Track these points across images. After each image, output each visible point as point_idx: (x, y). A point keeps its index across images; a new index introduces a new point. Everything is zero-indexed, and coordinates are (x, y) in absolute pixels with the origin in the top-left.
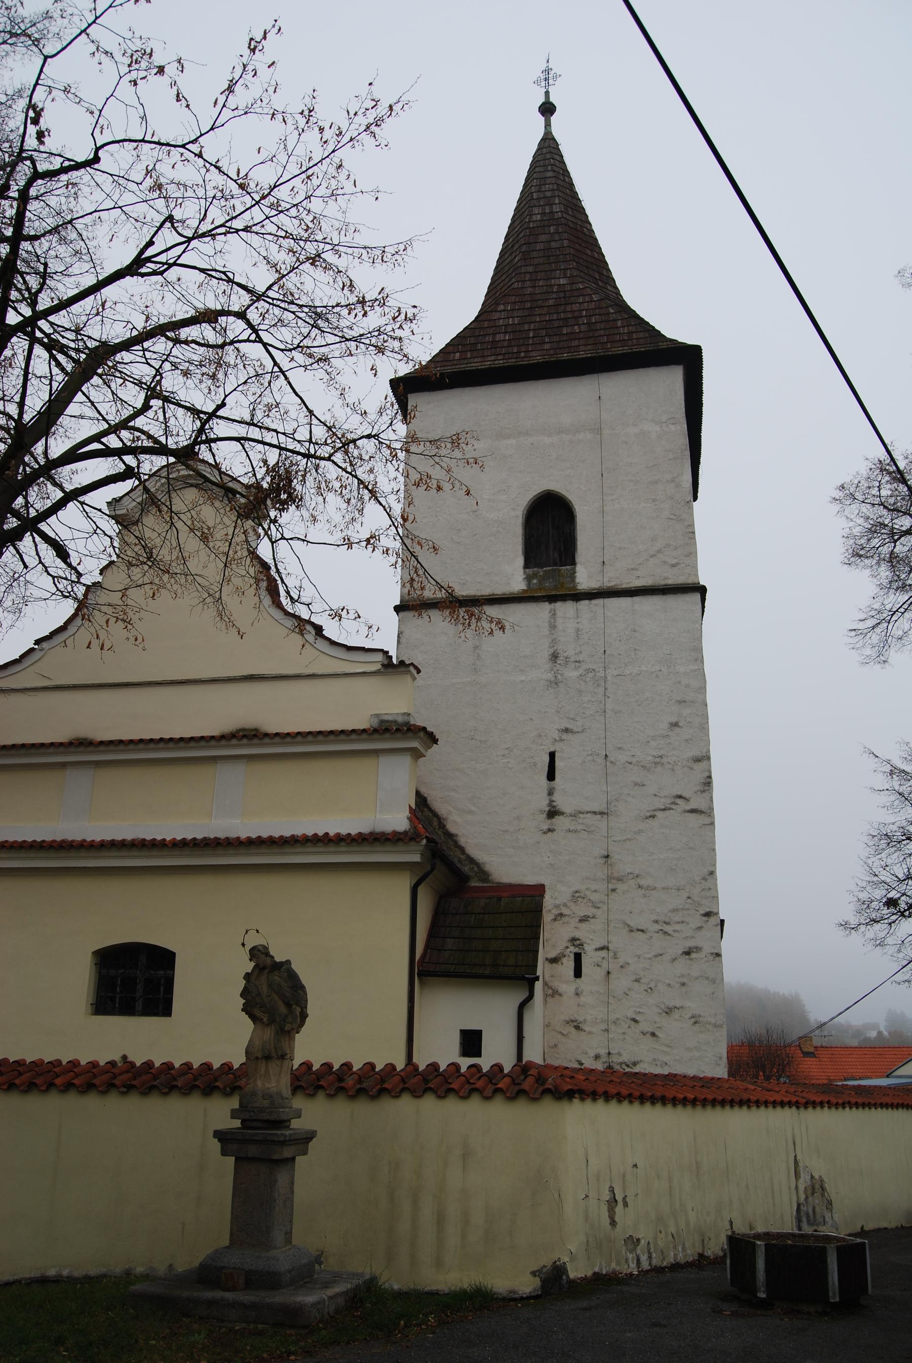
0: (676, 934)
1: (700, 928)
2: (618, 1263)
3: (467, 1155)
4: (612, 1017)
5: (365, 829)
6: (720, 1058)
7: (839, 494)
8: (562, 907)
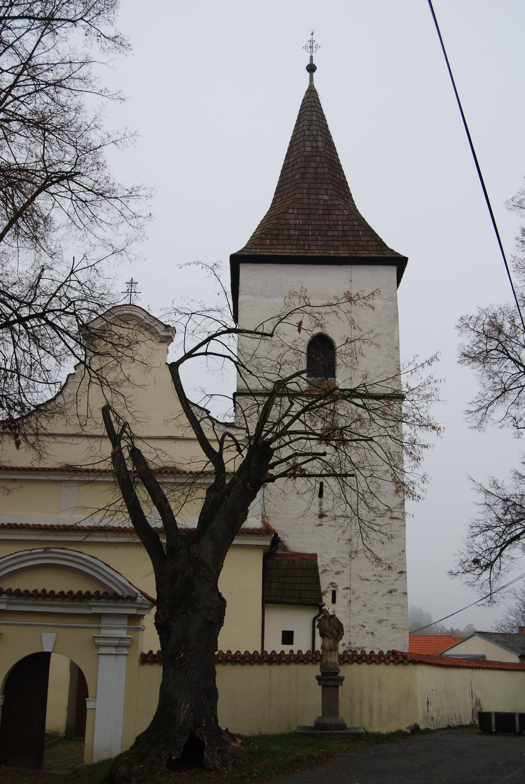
0: (384, 582)
1: (397, 579)
2: (430, 726)
3: (380, 686)
4: (352, 624)
6: (406, 646)
7: (458, 323)
8: (326, 566)
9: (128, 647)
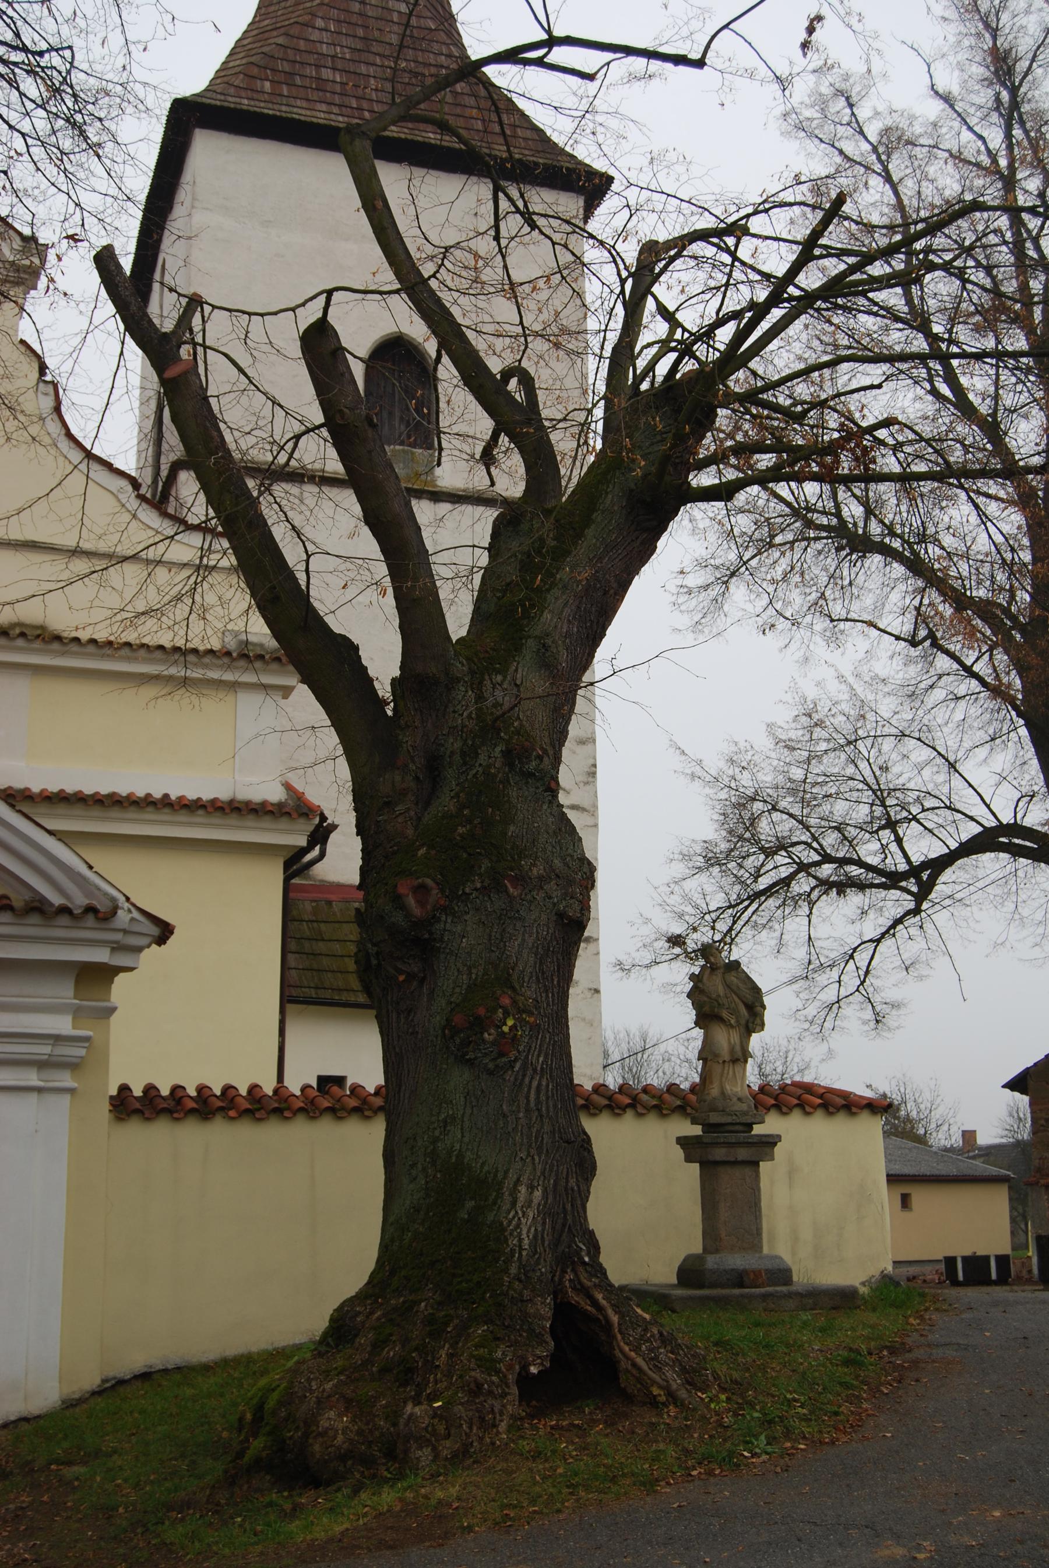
5: (224, 795)
9: (73, 1066)
